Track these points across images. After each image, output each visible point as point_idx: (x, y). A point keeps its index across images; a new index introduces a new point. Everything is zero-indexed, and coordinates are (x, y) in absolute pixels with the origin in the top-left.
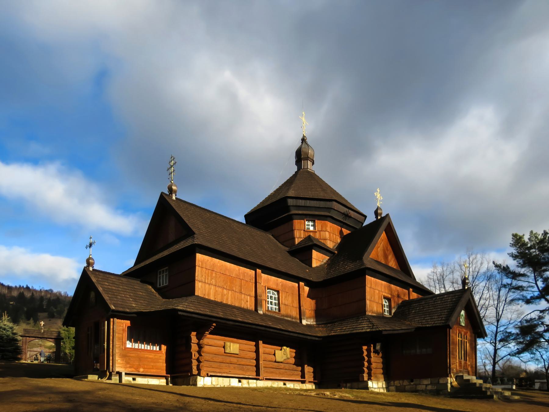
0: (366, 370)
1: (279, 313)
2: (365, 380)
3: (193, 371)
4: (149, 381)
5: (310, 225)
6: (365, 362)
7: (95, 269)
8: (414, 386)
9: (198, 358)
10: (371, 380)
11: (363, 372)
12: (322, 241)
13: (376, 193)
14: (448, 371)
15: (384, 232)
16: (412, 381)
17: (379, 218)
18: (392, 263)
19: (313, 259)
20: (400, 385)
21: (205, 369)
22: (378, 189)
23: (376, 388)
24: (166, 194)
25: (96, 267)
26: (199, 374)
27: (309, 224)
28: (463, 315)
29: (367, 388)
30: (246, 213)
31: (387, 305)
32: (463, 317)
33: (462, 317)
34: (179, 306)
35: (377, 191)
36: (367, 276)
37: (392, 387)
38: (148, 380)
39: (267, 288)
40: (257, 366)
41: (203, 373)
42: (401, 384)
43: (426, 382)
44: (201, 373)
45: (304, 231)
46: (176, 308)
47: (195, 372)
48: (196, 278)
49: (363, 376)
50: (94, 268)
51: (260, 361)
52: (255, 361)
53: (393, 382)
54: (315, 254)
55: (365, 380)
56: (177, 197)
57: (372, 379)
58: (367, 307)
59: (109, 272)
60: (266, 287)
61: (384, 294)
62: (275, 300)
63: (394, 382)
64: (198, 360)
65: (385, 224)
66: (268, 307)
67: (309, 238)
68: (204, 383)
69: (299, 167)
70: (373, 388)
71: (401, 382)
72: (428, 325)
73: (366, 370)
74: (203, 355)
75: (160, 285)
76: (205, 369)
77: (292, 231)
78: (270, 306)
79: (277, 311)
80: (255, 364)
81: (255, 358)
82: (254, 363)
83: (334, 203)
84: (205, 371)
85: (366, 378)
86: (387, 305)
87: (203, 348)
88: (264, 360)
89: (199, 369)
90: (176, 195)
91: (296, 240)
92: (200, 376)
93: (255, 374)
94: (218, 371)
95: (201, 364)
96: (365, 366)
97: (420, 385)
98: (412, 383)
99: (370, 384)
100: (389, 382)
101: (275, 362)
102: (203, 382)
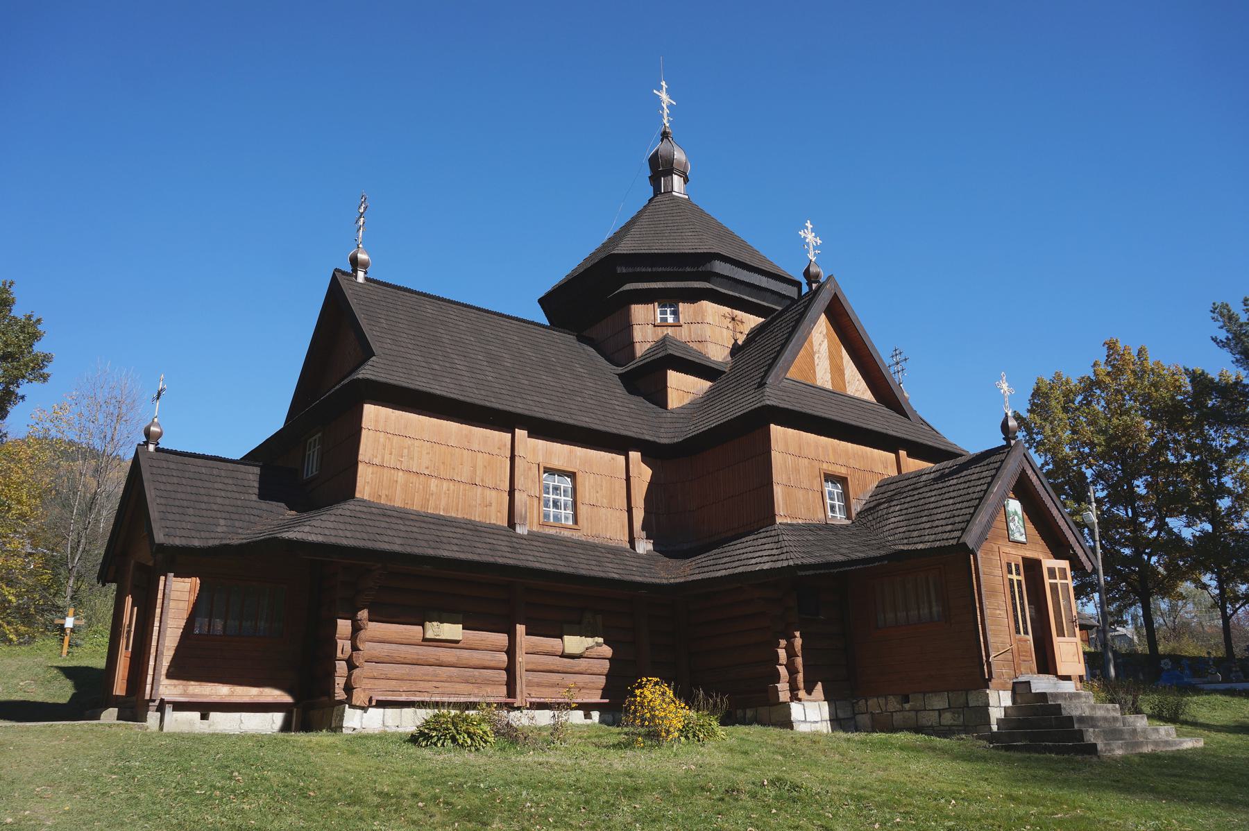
0: (783, 671)
1: (576, 527)
2: (781, 700)
3: (336, 691)
4: (274, 718)
5: (668, 312)
6: (779, 650)
7: (161, 447)
8: (912, 714)
9: (351, 656)
10: (800, 700)
11: (776, 677)
12: (694, 346)
13: (804, 232)
14: (986, 670)
15: (823, 316)
16: (906, 699)
17: (814, 286)
18: (857, 387)
19: (669, 390)
20: (880, 711)
21: (367, 684)
22: (808, 221)
23: (817, 722)
24: (344, 273)
25: (163, 444)
26: (349, 701)
27: (660, 314)
28: (1016, 513)
29: (787, 723)
30: (542, 294)
31: (837, 493)
32: (1016, 518)
33: (1013, 519)
34: (306, 523)
35: (807, 228)
36: (772, 426)
37: (864, 715)
38: (273, 716)
39: (545, 468)
40: (510, 670)
41: (359, 697)
42: (884, 709)
43: (939, 702)
44: (353, 698)
45: (655, 326)
46: (279, 535)
47: (340, 694)
48: (360, 458)
49: (776, 691)
50: (159, 446)
51: (517, 656)
52: (504, 657)
53: (864, 701)
54: (675, 379)
55: (781, 700)
56: (369, 276)
57: (799, 696)
58: (778, 505)
59: (193, 452)
60: (541, 465)
61: (825, 466)
62: (564, 496)
63: (866, 701)
64: (351, 666)
65: (824, 299)
66: (547, 516)
67: (664, 341)
68: (362, 722)
69: (657, 191)
70: (805, 721)
71: (882, 701)
72: (920, 546)
73: (783, 671)
74: (361, 648)
75: (307, 475)
76: (367, 684)
77: (629, 327)
78: (552, 510)
79: (570, 523)
80: (505, 665)
81: (505, 649)
82: (504, 662)
83: (717, 263)
84: (364, 690)
85: (784, 696)
86: (837, 493)
87: (362, 631)
88: (527, 651)
89: (349, 689)
90: (366, 273)
91: (637, 346)
92: (353, 707)
93: (504, 689)
94: (405, 689)
95: (356, 672)
96: (780, 662)
97: (926, 710)
98: (907, 706)
99: (796, 710)
100: (855, 701)
101: (563, 656)
102: (353, 720)
